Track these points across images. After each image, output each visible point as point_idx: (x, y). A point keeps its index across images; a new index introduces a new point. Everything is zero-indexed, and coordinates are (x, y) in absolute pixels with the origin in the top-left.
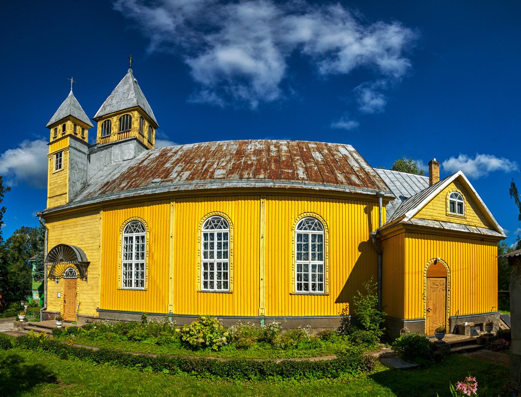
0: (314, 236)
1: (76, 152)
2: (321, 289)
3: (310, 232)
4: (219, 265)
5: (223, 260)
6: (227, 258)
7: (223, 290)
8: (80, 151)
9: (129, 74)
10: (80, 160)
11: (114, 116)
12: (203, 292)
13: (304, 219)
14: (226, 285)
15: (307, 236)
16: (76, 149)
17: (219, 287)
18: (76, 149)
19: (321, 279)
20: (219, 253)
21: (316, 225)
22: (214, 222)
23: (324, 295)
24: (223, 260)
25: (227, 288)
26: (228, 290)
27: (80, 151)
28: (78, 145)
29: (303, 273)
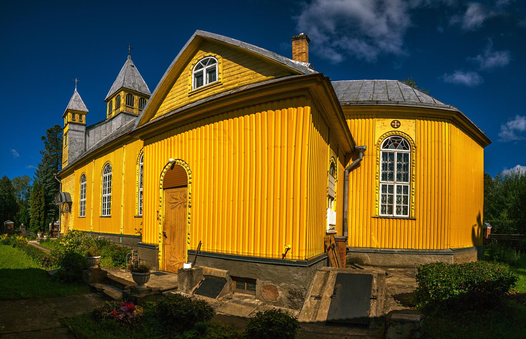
0: (399, 155)
1: (74, 132)
2: (405, 213)
3: (396, 151)
4: (399, 188)
5: (403, 184)
6: (407, 181)
7: (402, 216)
8: (78, 131)
9: (129, 63)
10: (77, 137)
11: (113, 97)
12: (381, 218)
13: (389, 138)
14: (109, 211)
15: (392, 154)
16: (75, 130)
17: (398, 212)
18: (75, 130)
19: (406, 202)
20: (399, 176)
21: (402, 144)
22: (393, 141)
23: (408, 219)
24: (389, 183)
25: (407, 214)
26: (408, 216)
27: (78, 131)
28: (76, 127)
29: (402, 195)
